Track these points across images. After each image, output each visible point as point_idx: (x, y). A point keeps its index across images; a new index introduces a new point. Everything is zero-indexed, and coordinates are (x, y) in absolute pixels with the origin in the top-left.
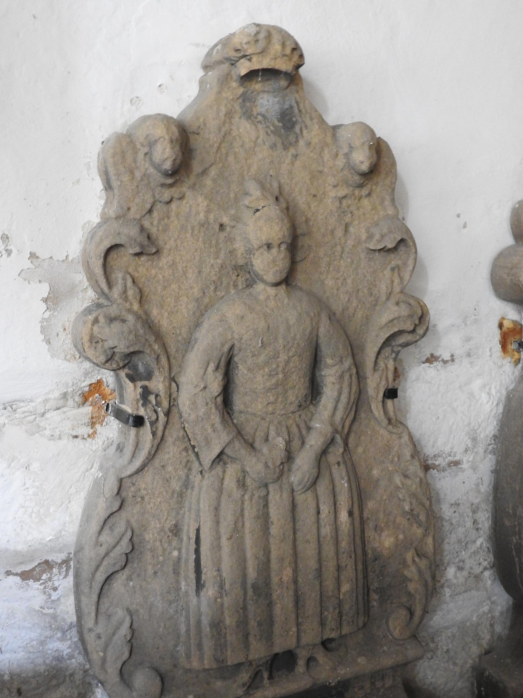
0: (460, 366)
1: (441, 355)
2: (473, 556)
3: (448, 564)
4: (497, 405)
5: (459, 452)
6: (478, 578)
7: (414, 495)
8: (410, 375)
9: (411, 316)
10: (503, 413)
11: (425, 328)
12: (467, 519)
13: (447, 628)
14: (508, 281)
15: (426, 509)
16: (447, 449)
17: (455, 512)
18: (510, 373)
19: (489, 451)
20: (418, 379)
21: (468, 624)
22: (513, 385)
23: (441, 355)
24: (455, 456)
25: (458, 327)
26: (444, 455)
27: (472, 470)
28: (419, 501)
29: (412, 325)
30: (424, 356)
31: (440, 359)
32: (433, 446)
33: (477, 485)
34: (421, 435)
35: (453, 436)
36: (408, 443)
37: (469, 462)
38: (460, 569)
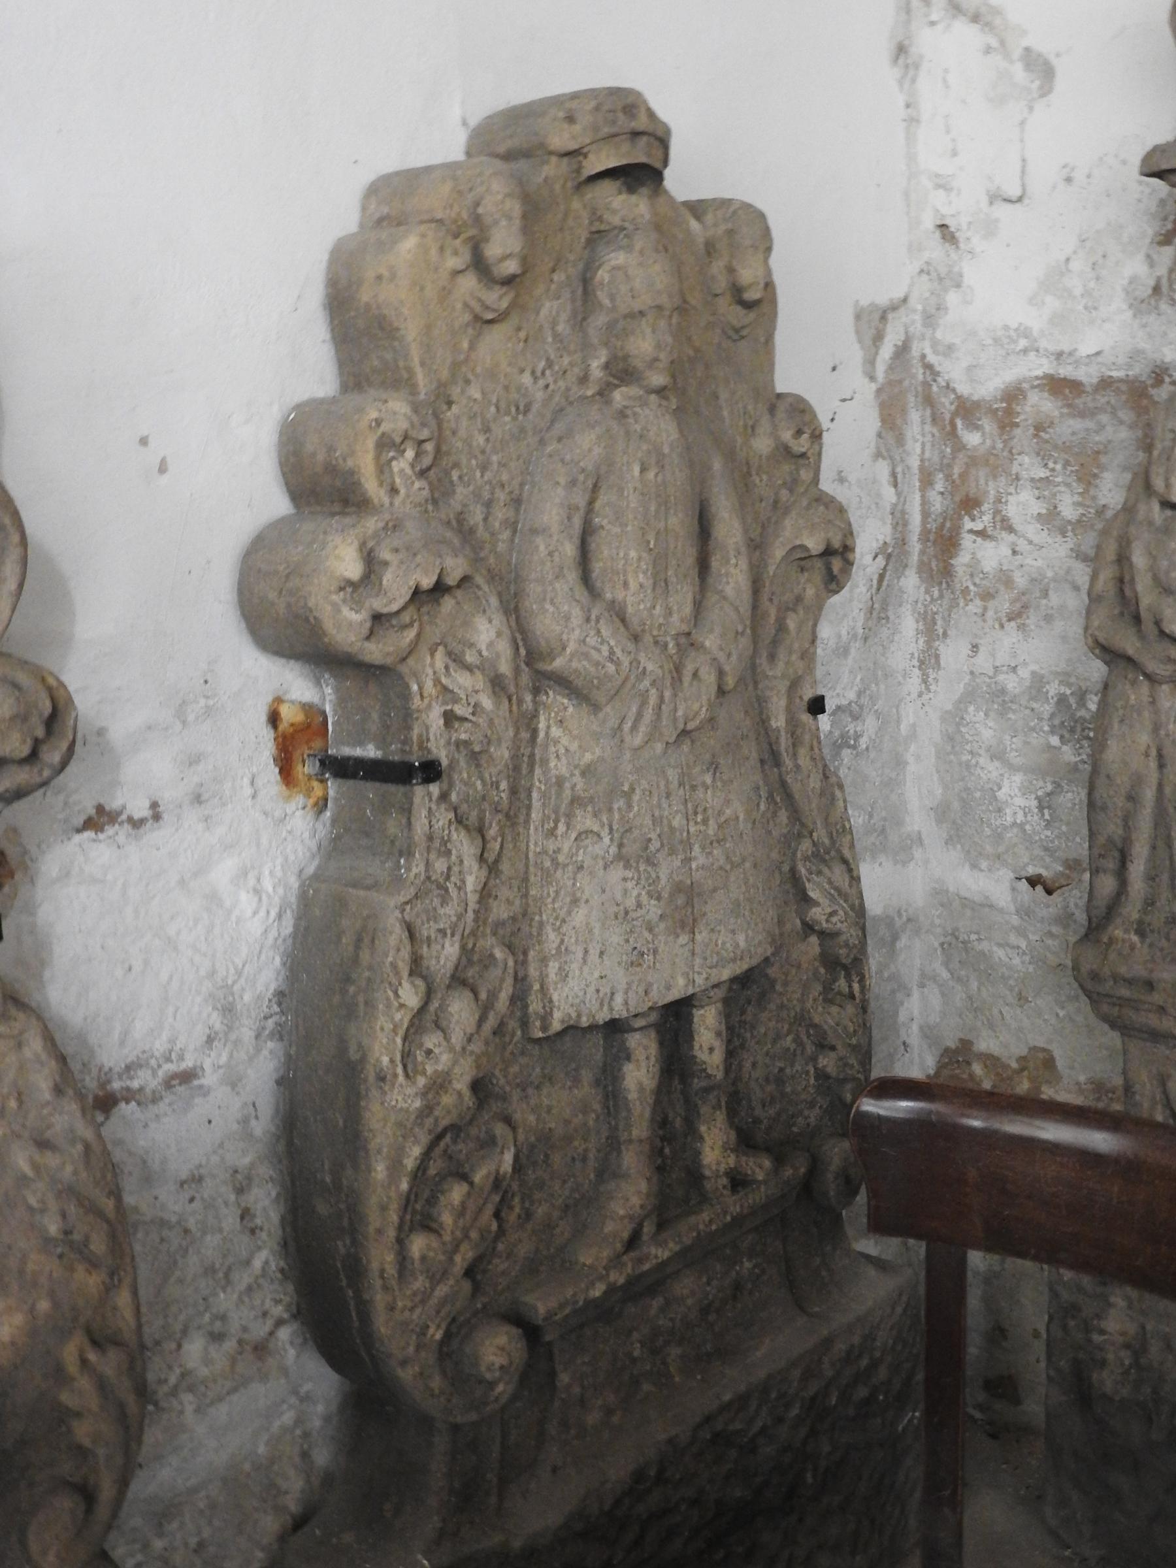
0: (177, 830)
1: (124, 807)
2: (246, 1299)
3: (185, 1331)
4: (280, 916)
5: (191, 1047)
6: (261, 1349)
7: (69, 1192)
8: (43, 868)
9: (20, 718)
10: (294, 935)
11: (64, 745)
12: (224, 1211)
13: (194, 1490)
14: (281, 608)
15: (108, 1221)
16: (159, 1046)
17: (192, 1200)
18: (306, 835)
19: (267, 1032)
20: (66, 874)
21: (247, 1467)
22: (316, 863)
23: (124, 807)
24: (181, 1058)
25: (166, 729)
26: (153, 1062)
27: (229, 1088)
28: (86, 1202)
29: (24, 742)
30: (79, 812)
31: (124, 817)
32: (122, 1043)
33: (245, 1121)
34: (85, 1019)
35: (171, 1010)
36: (44, 1057)
37: (219, 1067)
38: (217, 1337)
